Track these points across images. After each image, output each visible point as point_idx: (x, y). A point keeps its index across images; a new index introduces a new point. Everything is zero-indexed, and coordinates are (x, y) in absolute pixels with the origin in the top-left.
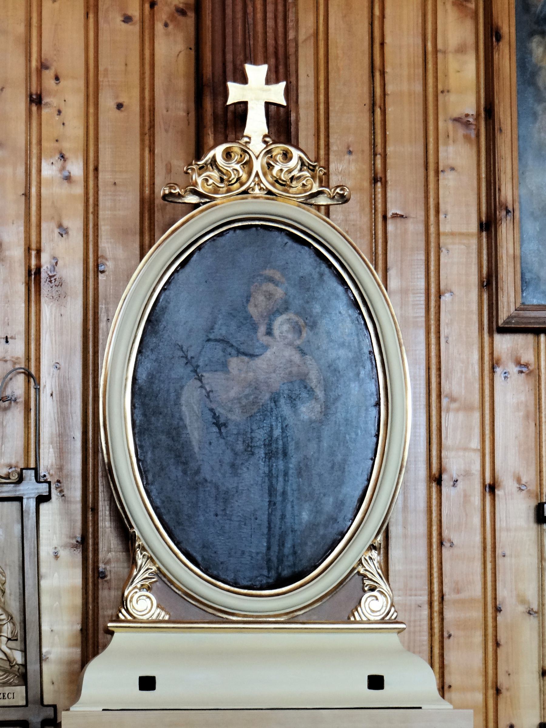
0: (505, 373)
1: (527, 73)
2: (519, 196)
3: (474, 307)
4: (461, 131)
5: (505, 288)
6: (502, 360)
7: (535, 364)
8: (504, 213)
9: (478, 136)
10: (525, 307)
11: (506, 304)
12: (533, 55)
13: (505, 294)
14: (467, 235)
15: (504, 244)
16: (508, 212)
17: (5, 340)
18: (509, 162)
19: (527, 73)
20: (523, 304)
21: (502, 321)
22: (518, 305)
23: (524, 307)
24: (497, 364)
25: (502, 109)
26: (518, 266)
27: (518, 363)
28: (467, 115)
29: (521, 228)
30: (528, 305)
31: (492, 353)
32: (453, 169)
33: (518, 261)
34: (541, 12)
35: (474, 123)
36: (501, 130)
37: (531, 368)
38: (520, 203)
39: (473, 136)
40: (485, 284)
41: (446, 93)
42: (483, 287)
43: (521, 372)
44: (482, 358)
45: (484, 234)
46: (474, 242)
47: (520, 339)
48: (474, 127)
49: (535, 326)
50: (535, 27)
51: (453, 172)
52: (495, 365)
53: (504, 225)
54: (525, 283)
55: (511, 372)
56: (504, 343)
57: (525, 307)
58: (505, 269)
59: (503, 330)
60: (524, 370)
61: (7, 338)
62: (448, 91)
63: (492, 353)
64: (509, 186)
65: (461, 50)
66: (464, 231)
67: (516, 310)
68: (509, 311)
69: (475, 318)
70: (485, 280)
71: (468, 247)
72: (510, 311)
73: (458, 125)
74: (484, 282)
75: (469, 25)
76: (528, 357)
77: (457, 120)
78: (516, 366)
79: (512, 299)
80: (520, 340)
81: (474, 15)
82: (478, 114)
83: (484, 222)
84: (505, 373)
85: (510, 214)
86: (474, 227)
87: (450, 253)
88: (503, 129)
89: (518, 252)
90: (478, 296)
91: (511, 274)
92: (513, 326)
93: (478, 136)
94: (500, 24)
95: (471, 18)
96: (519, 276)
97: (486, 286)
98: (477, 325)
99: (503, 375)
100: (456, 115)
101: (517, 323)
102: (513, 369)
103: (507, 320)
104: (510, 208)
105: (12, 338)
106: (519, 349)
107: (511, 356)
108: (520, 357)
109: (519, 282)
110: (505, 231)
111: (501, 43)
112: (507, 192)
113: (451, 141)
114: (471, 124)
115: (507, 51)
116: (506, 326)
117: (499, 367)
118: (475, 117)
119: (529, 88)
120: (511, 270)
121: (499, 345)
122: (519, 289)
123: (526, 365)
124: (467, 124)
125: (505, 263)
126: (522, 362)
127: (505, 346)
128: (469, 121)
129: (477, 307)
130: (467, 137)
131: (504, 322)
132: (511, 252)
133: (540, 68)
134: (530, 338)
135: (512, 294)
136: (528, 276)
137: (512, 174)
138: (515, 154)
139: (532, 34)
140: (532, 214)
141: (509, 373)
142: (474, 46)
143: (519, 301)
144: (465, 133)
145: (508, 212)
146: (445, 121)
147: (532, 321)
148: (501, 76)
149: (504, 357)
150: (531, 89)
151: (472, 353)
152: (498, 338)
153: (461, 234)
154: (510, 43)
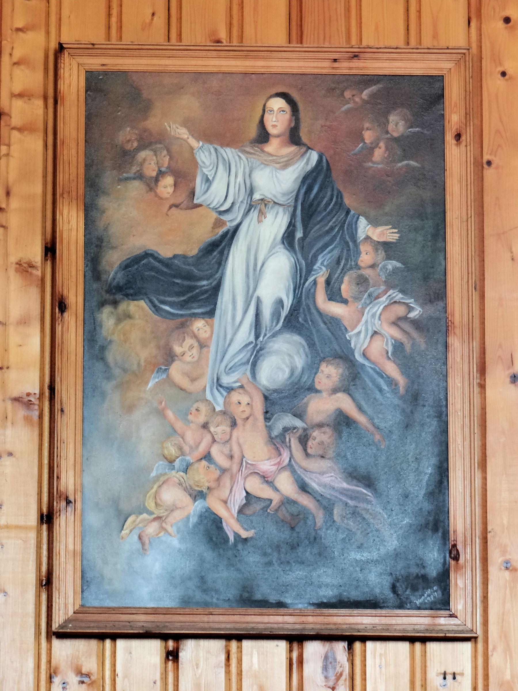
0: (64, 683)
1: (95, 346)
2: (82, 485)
3: (31, 608)
4: (21, 412)
5: (62, 589)
6: (61, 669)
7: (98, 673)
8: (63, 504)
9: (41, 417)
10: (85, 609)
11: (62, 606)
12: (103, 326)
13: (62, 594)
14: (25, 528)
15: (63, 538)
16: (68, 502)
17: (442, 676)
18: (71, 446)
19: (95, 346)
20: (82, 606)
21: (57, 625)
22: (77, 607)
23: (83, 610)
24: (55, 673)
25: (64, 388)
26: (79, 563)
27: (79, 672)
28: (28, 395)
29: (82, 521)
30: (89, 607)
31: (49, 662)
32: (10, 454)
33: (78, 558)
34: (114, 279)
35: (37, 402)
36: (62, 411)
37: (93, 678)
38: (82, 492)
39: (36, 418)
40: (44, 583)
41: (5, 370)
42: (42, 586)
43: (83, 682)
44: (38, 666)
45: (45, 527)
46: (32, 535)
47: (81, 644)
48: (36, 407)
49: (94, 631)
50: (107, 296)
51: (11, 457)
52: (53, 674)
53: (63, 517)
54: (85, 582)
55: (70, 683)
56: (63, 649)
57: (85, 609)
58: (63, 565)
59: (62, 635)
60: (86, 680)
61: (454, 674)
62: (8, 368)
63: (49, 662)
64: (71, 473)
65: (24, 322)
66: (22, 523)
67: (74, 613)
68: (66, 613)
69: (31, 621)
70: (44, 579)
71: (25, 542)
72: (68, 614)
73: (17, 404)
74: (42, 581)
75: (34, 293)
76: (90, 665)
77: (17, 400)
78: (77, 675)
79: (71, 600)
80: (81, 646)
81: (40, 283)
82: (42, 394)
83: (45, 513)
84: (64, 683)
85: (71, 504)
86: (33, 519)
87: (4, 548)
88: (65, 410)
89: (78, 548)
90: (36, 596)
91: (70, 573)
92: (69, 630)
93: (41, 417)
94: (65, 293)
95: (37, 287)
96: (79, 574)
97: (45, 585)
98: (33, 629)
99: (61, 686)
100: (15, 394)
101: (75, 627)
102: (73, 679)
103: (64, 624)
104: (71, 498)
105: (459, 674)
106: (80, 657)
107: (72, 663)
108: (81, 666)
109: (79, 582)
110: (65, 523)
111: (66, 315)
112: (68, 481)
113: (9, 424)
114: (34, 404)
115: (73, 323)
116: (61, 631)
117: (57, 676)
118: (38, 396)
119: (97, 364)
120: (70, 567)
121: (58, 652)
122: (79, 589)
123: (88, 675)
124: (29, 404)
125: (63, 559)
126: (84, 671)
127: (64, 653)
128: (30, 401)
129: (34, 610)
130: (28, 419)
131: (59, 626)
132: (71, 547)
133: (111, 342)
134: (94, 643)
135: (71, 594)
136: (89, 575)
137: (75, 461)
138: (79, 438)
139: (102, 304)
140: (97, 504)
141: (68, 683)
142: (39, 317)
143: (79, 602)
144: (26, 414)
145: (68, 502)
146: (4, 400)
147: (92, 625)
148: (65, 352)
149: (63, 666)
150: (99, 366)
151: (27, 660)
152: (56, 643)
153: (18, 527)
154: (76, 314)
